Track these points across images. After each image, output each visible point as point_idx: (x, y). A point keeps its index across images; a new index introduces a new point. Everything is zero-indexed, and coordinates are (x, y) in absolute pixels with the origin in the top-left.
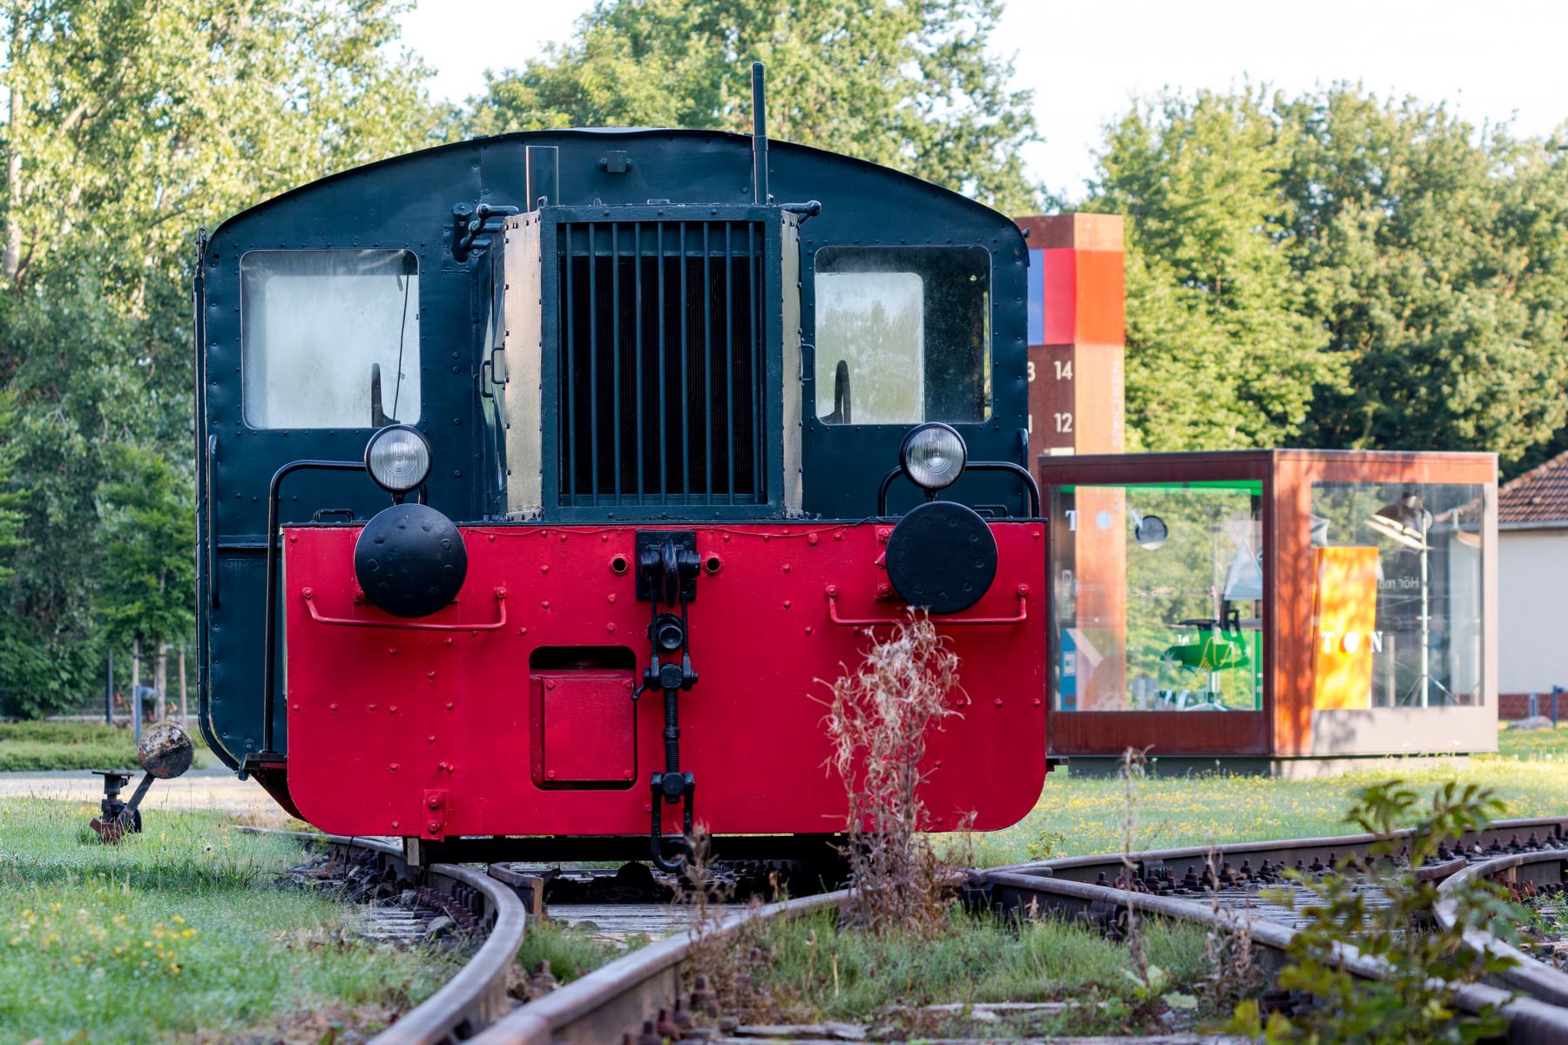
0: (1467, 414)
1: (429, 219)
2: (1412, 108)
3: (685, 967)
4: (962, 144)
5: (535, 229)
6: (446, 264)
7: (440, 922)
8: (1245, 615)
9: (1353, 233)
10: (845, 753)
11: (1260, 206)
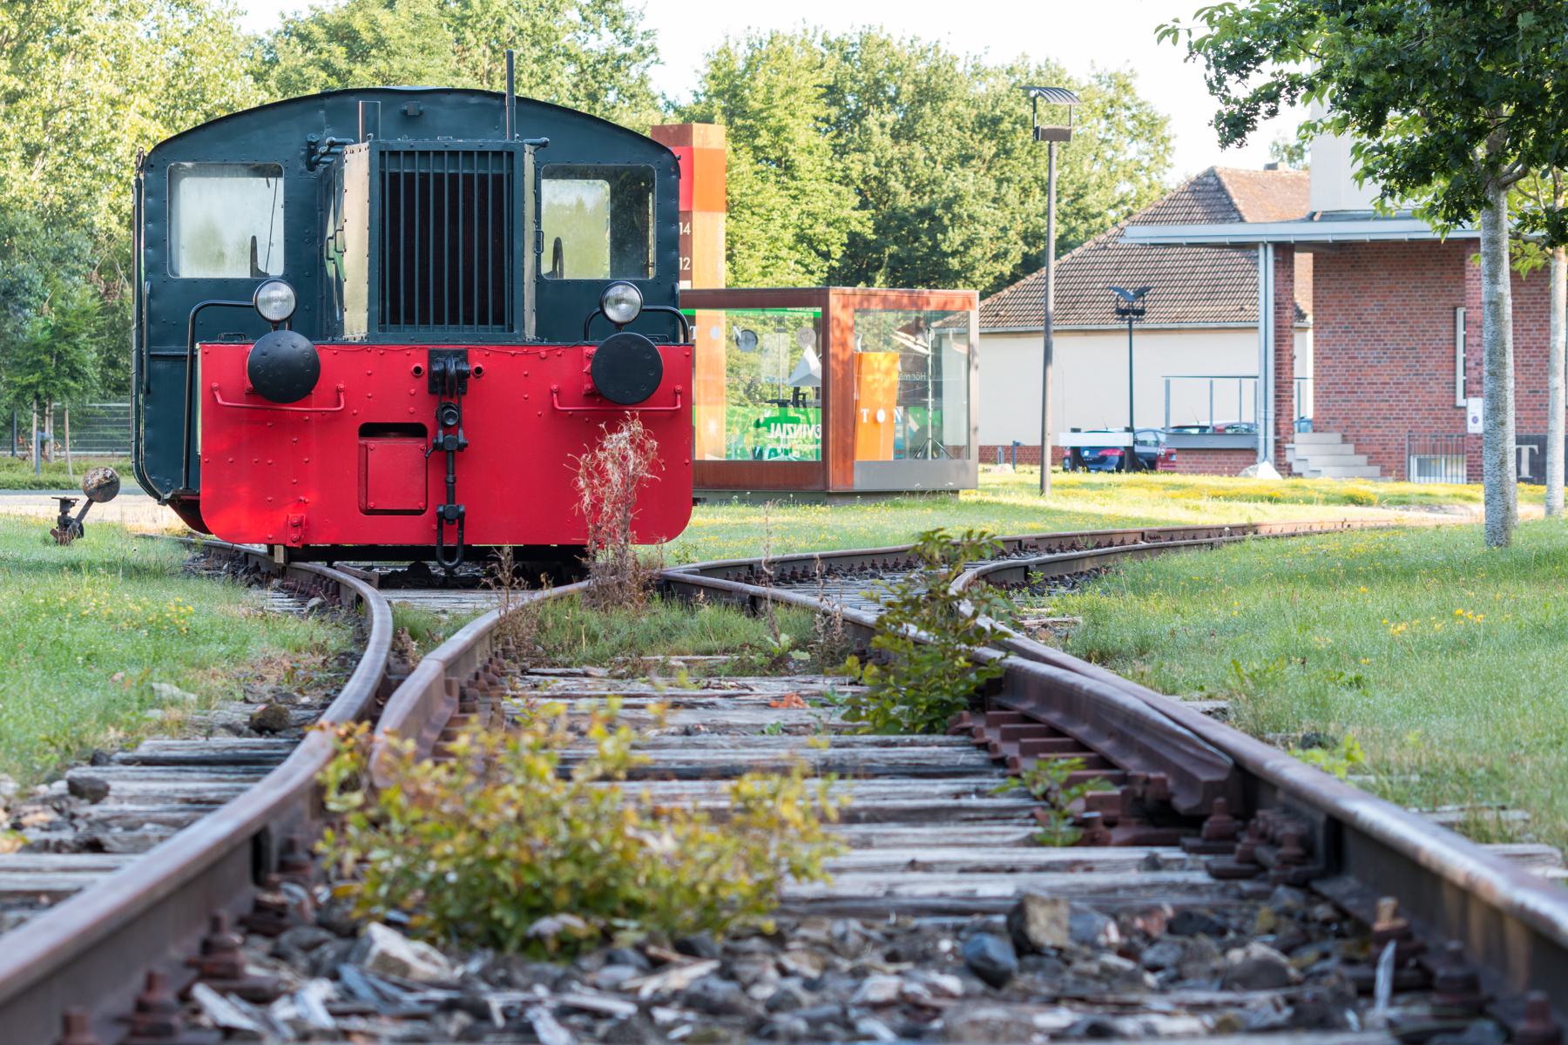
0: (954, 254)
1: (290, 142)
2: (916, 44)
3: (495, 633)
5: (365, 155)
6: (302, 173)
7: (315, 601)
8: (811, 397)
9: (876, 129)
10: (587, 499)
11: (813, 110)
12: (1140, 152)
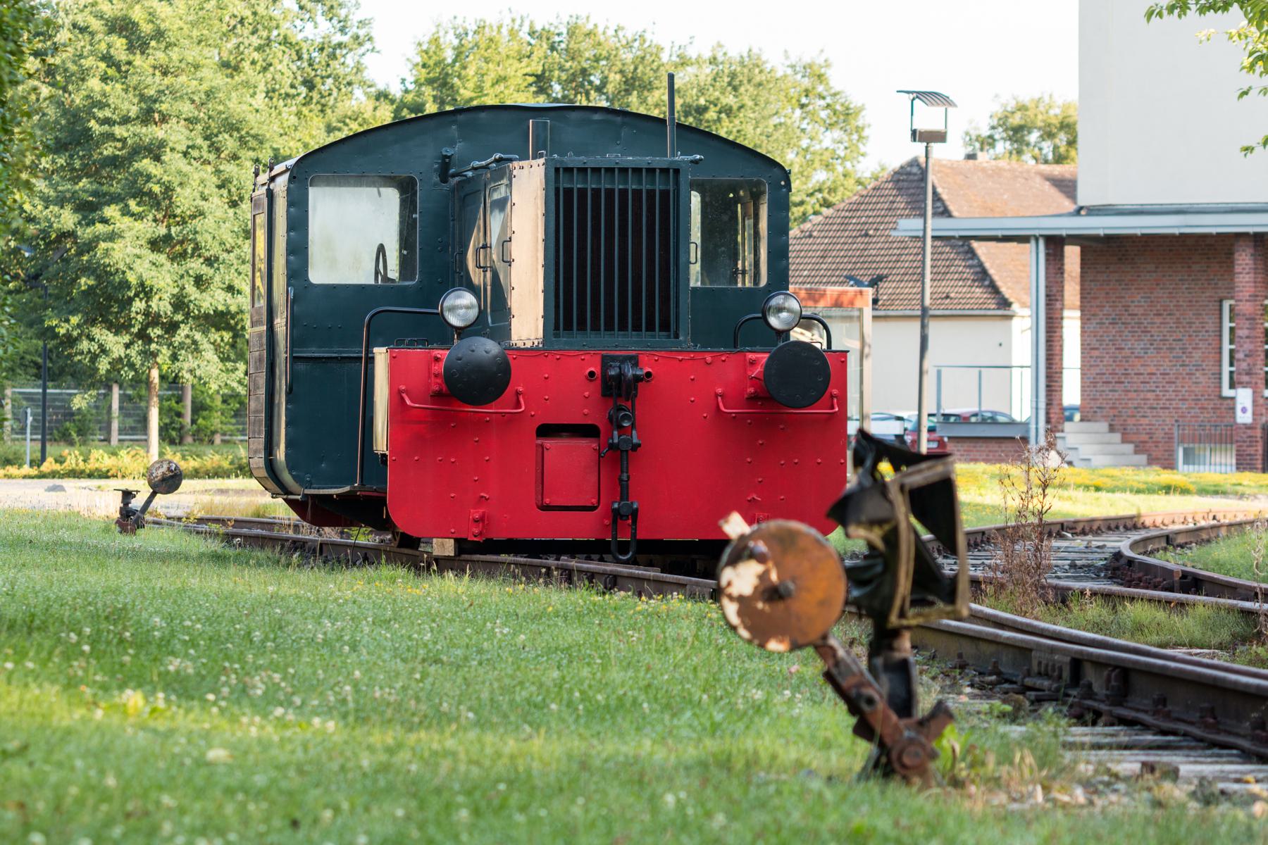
1: (420, 160)
2: (620, 34)
4: (325, 52)
6: (435, 184)
12: (834, 141)
